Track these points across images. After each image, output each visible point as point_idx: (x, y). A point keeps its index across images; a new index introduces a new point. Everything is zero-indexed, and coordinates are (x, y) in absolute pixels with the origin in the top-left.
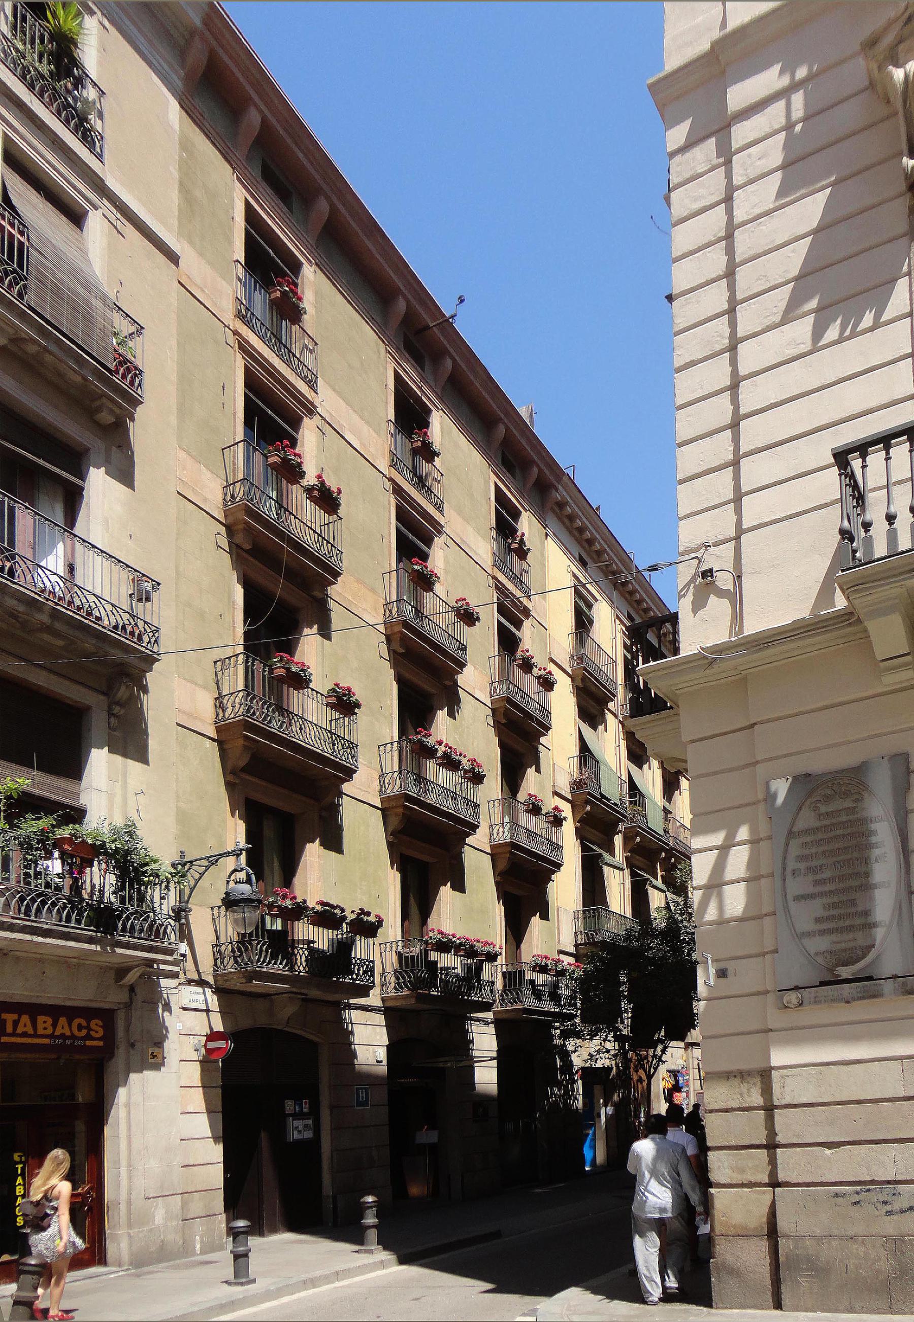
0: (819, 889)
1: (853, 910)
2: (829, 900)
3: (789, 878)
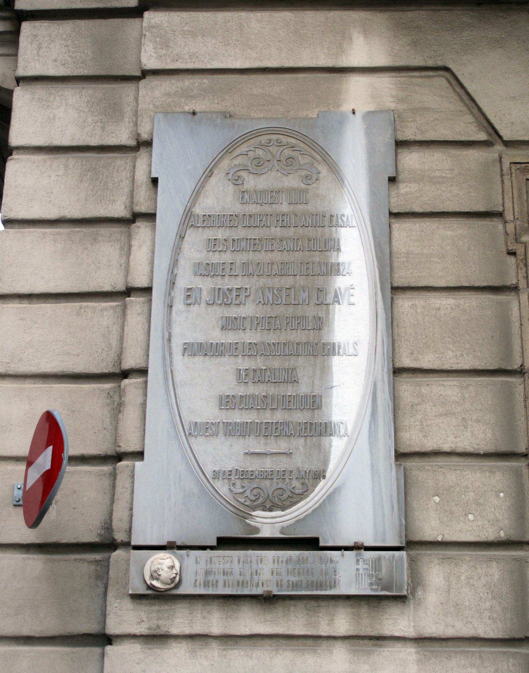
0: (230, 338)
1: (289, 390)
2: (244, 363)
3: (179, 305)
